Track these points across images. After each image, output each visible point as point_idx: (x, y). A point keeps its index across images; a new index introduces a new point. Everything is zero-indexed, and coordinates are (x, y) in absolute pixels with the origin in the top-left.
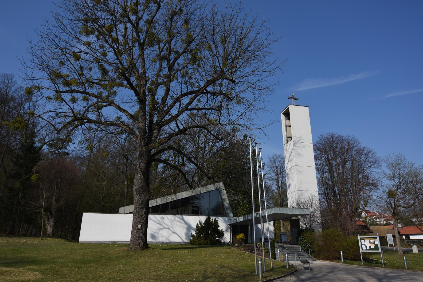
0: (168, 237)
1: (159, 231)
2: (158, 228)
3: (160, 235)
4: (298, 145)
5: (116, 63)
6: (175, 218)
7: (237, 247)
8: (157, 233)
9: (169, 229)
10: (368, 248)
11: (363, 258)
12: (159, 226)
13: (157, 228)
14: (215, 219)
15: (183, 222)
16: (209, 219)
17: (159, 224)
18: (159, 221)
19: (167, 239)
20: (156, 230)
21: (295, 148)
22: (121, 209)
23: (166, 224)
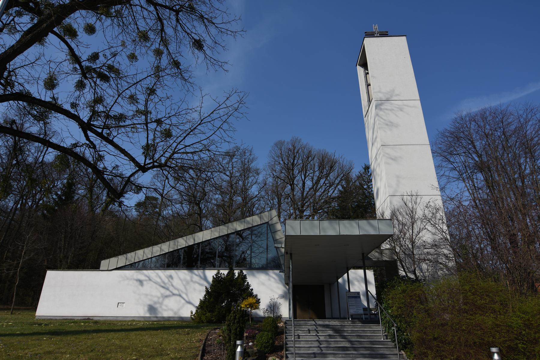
0: (179, 310)
1: (163, 299)
2: (162, 294)
3: (164, 307)
4: (386, 107)
6: (192, 277)
8: (159, 303)
9: (180, 296)
12: (163, 291)
13: (159, 295)
16: (231, 273)
17: (163, 287)
18: (164, 283)
19: (152, 309)
20: (159, 298)
21: (381, 113)
22: (104, 263)
23: (176, 289)
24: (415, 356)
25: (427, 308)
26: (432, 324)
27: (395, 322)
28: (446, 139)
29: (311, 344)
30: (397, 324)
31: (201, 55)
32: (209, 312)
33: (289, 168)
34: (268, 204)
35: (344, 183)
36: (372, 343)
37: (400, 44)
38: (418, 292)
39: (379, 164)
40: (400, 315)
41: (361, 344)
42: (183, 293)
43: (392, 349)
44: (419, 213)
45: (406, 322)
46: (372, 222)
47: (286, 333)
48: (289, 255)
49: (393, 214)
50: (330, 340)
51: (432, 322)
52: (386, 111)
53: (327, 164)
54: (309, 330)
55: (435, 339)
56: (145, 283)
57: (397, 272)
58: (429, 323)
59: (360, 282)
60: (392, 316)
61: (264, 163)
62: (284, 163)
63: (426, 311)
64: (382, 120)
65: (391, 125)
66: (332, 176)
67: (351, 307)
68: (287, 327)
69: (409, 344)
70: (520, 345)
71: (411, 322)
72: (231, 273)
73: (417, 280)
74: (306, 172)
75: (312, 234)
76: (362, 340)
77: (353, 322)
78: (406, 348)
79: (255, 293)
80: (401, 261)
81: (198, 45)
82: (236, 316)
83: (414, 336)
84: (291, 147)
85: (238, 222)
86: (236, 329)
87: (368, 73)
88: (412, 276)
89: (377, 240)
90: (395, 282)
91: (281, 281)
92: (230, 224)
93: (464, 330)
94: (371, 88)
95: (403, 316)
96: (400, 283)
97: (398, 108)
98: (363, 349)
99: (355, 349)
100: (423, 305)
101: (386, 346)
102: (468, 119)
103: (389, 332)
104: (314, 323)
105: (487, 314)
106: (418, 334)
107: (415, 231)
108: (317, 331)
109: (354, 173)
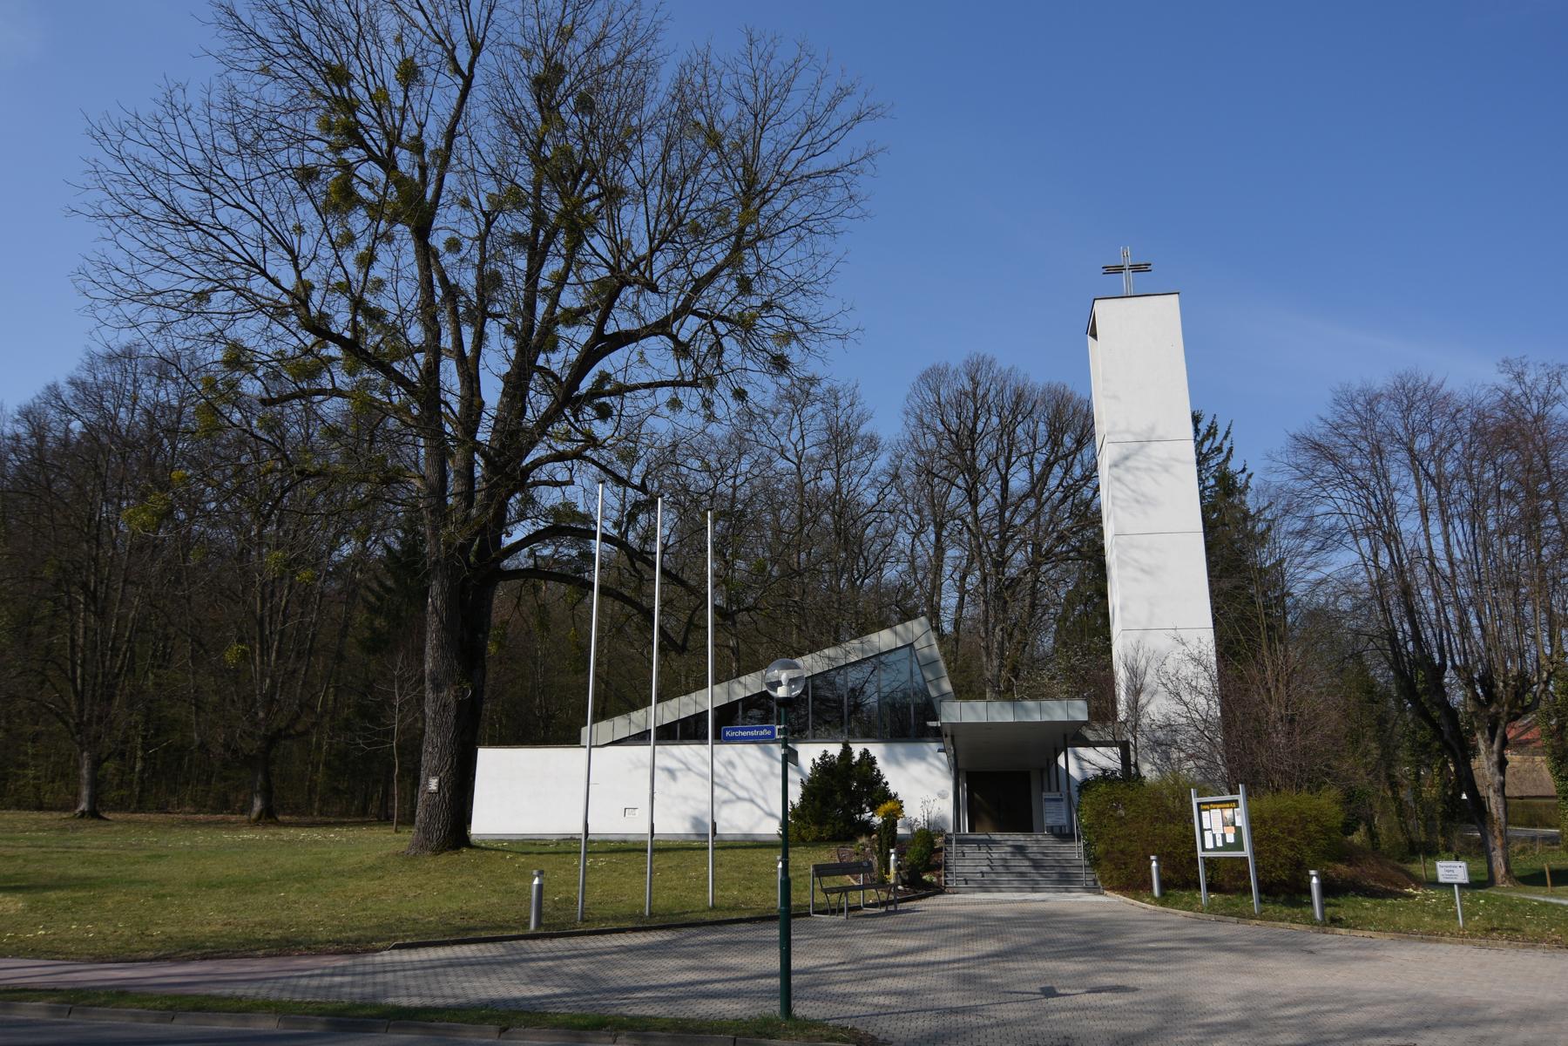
5: (708, 292)
7: (1226, 878)
9: (752, 801)
10: (1219, 844)
11: (1259, 882)
16: (847, 752)
23: (742, 787)
33: (964, 442)
42: (745, 790)
56: (679, 774)
72: (847, 752)
75: (999, 720)
79: (892, 789)
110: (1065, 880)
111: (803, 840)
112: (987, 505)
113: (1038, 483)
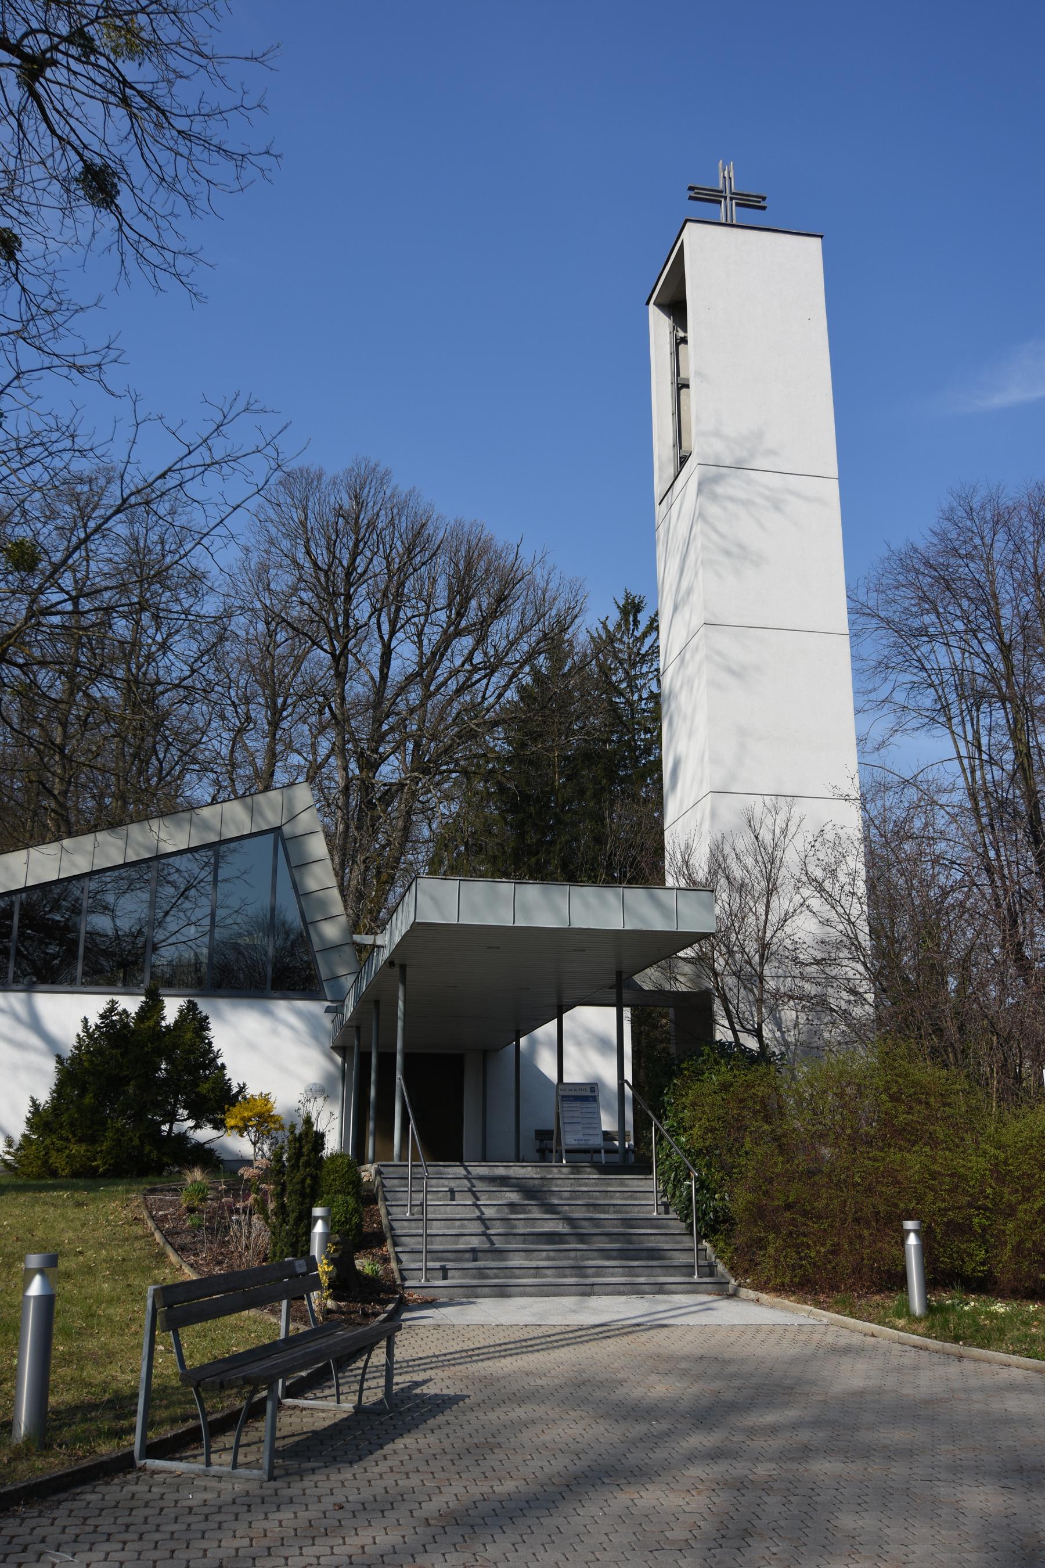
4: (731, 492)
14: (192, 1007)
15: (35, 1040)
21: (713, 510)
24: (736, 1249)
25: (779, 1131)
26: (787, 1170)
27: (694, 1166)
28: (911, 576)
29: (462, 1227)
30: (699, 1171)
31: (109, 221)
32: (80, 1141)
33: (334, 587)
34: (223, 717)
35: (541, 660)
36: (627, 1222)
37: (795, 264)
38: (760, 1091)
39: (689, 682)
40: (709, 1151)
41: (598, 1227)
43: (678, 1238)
44: (791, 858)
45: (722, 1168)
46: (660, 893)
47: (386, 1200)
48: (396, 970)
49: (718, 865)
50: (514, 1216)
51: (788, 1166)
52: (730, 505)
53: (481, 584)
54: (452, 1192)
55: (788, 1207)
57: (711, 1033)
58: (779, 1169)
59: (587, 1048)
60: (688, 1152)
61: (232, 555)
62: (315, 563)
63: (775, 1139)
64: (714, 536)
65: (738, 554)
66: (501, 630)
67: (568, 1128)
68: (386, 1182)
69: (725, 1221)
70: (976, 1220)
71: (734, 1167)
73: (764, 1055)
74: (398, 610)
76: (602, 1216)
77: (575, 1168)
78: (715, 1231)
80: (725, 1001)
81: (99, 183)
82: (301, 1147)
83: (737, 1200)
84: (347, 503)
85: (167, 821)
86: (303, 1181)
87: (684, 340)
88: (751, 1043)
89: (663, 946)
90: (704, 1062)
91: (316, 1038)
92: (134, 829)
93: (855, 1185)
94: (692, 398)
95: (717, 1152)
96: (718, 1063)
97: (768, 498)
98: (604, 1238)
99: (582, 1238)
100: (770, 1123)
101: (663, 1231)
102: (988, 515)
103: (673, 1196)
104: (461, 1171)
105: (916, 1148)
106: (750, 1197)
107: (773, 918)
108: (474, 1193)
109: (582, 635)
110: (634, 1255)
111: (54, 1173)
112: (357, 689)
113: (428, 665)
